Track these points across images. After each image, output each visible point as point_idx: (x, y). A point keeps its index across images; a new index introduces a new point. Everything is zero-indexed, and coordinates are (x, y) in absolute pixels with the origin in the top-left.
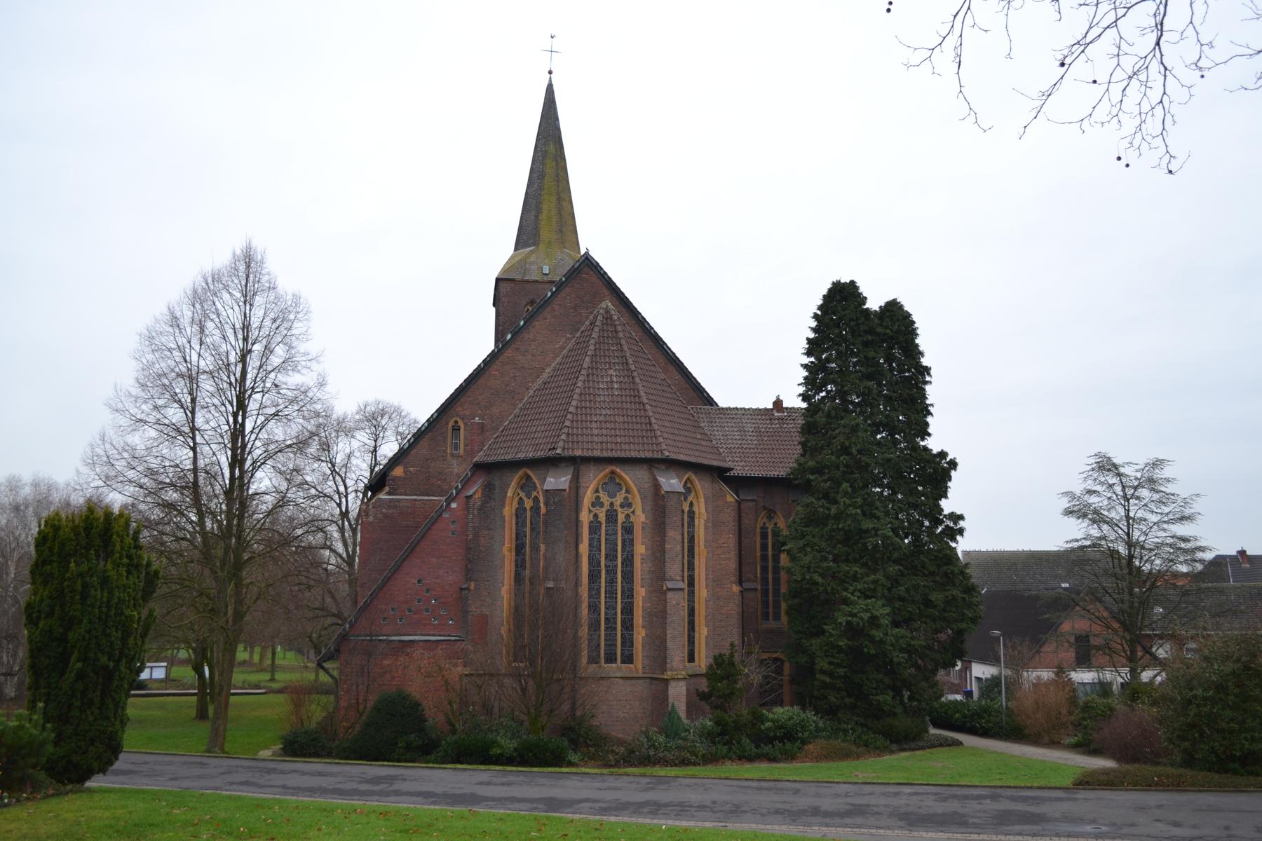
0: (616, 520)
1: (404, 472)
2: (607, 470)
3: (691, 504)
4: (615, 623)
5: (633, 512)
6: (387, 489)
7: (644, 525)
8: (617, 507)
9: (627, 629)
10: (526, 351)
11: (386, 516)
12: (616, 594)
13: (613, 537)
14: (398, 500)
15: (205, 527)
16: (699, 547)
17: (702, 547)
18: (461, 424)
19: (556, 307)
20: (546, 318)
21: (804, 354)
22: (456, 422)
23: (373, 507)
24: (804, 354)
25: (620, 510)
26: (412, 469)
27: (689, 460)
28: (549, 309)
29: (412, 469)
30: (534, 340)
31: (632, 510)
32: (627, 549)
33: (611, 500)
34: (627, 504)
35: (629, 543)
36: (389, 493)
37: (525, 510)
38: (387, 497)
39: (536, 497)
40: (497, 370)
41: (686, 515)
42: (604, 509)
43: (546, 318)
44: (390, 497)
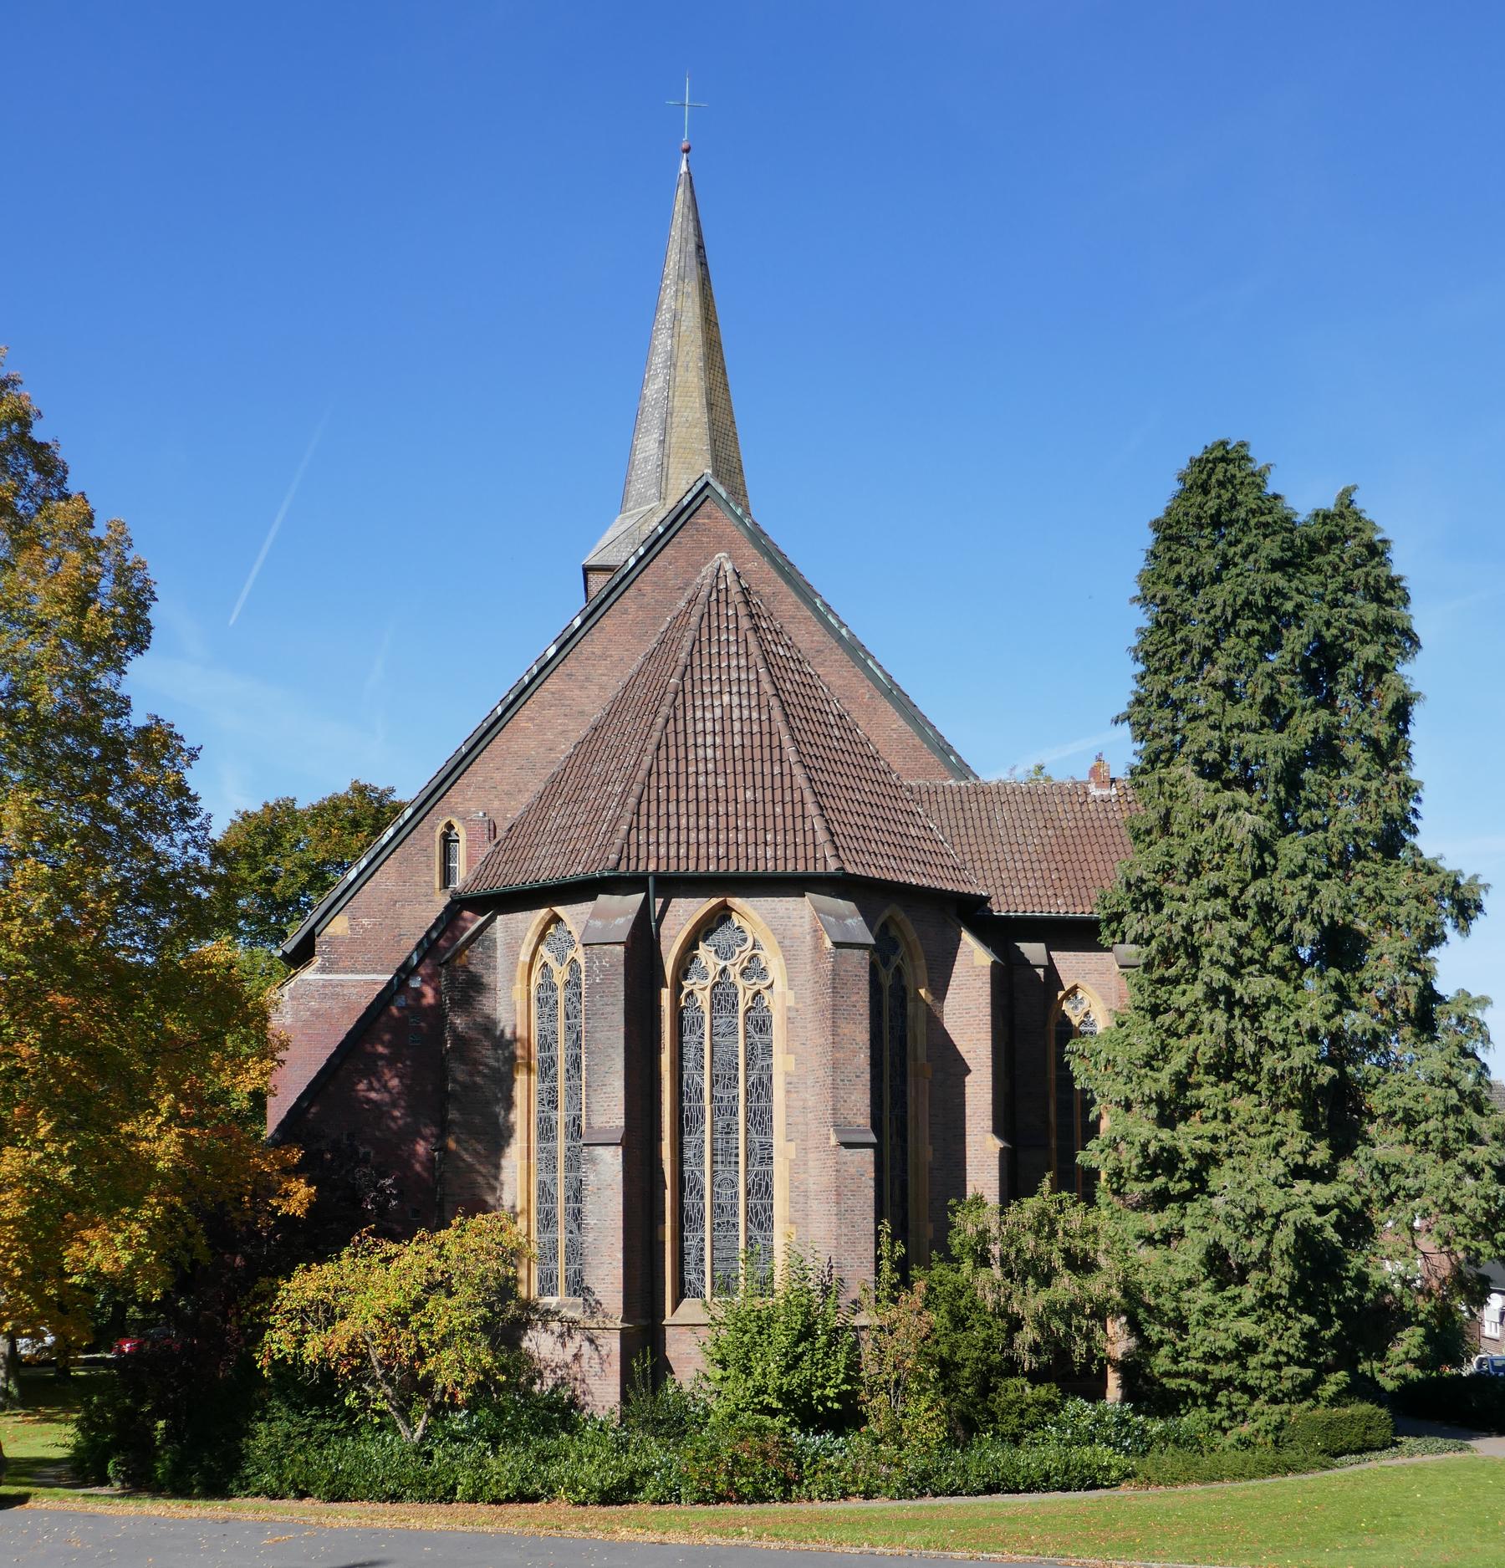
0: (735, 1005)
1: (352, 927)
2: (715, 901)
3: (898, 970)
4: (735, 1214)
5: (770, 987)
6: (317, 961)
7: (793, 1014)
8: (734, 972)
9: (761, 1225)
10: (587, 679)
11: (316, 1014)
12: (737, 1155)
13: (731, 1038)
14: (341, 984)
15: (1381, 746)
16: (916, 1060)
17: (922, 1060)
18: (459, 827)
19: (647, 589)
20: (626, 612)
21: (1135, 599)
22: (450, 826)
23: (292, 998)
24: (1135, 599)
25: (741, 983)
26: (365, 921)
27: (874, 873)
28: (632, 592)
29: (365, 921)
30: (604, 657)
31: (768, 983)
32: (759, 1063)
33: (722, 963)
34: (754, 969)
35: (759, 1054)
36: (323, 970)
37: (553, 989)
38: (319, 976)
39: (574, 960)
40: (531, 719)
41: (886, 993)
42: (709, 982)
43: (626, 612)
44: (325, 977)
